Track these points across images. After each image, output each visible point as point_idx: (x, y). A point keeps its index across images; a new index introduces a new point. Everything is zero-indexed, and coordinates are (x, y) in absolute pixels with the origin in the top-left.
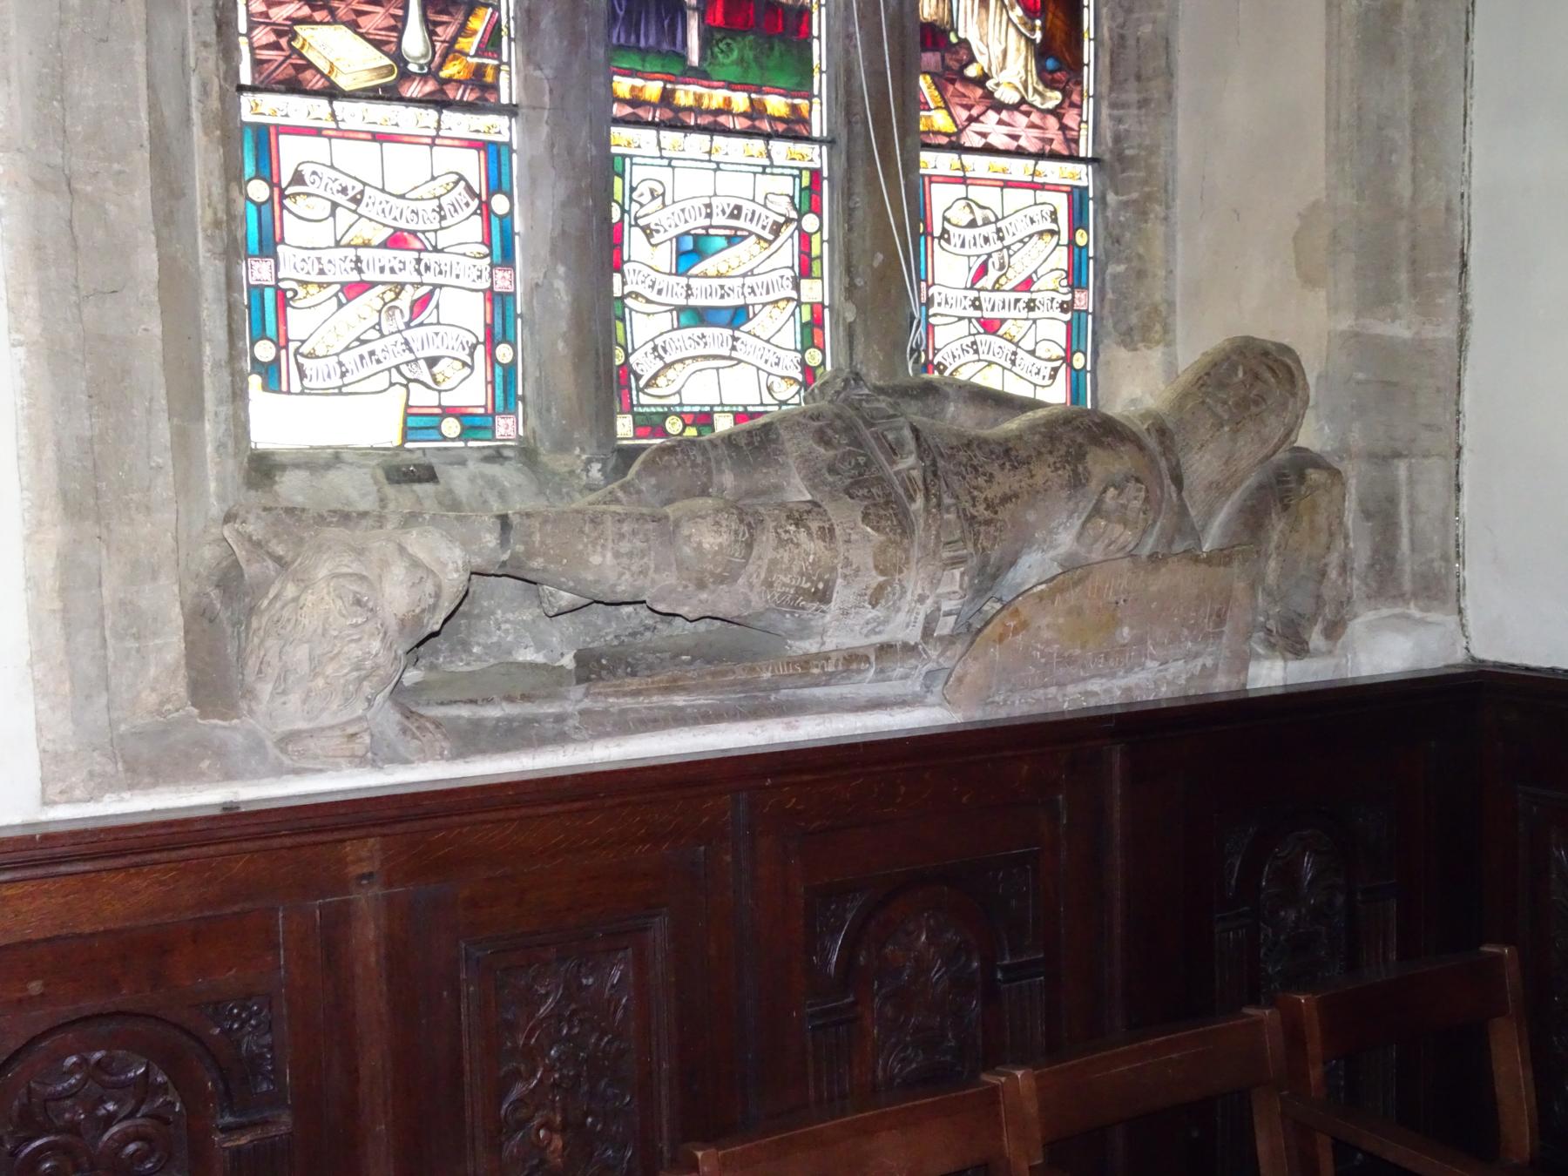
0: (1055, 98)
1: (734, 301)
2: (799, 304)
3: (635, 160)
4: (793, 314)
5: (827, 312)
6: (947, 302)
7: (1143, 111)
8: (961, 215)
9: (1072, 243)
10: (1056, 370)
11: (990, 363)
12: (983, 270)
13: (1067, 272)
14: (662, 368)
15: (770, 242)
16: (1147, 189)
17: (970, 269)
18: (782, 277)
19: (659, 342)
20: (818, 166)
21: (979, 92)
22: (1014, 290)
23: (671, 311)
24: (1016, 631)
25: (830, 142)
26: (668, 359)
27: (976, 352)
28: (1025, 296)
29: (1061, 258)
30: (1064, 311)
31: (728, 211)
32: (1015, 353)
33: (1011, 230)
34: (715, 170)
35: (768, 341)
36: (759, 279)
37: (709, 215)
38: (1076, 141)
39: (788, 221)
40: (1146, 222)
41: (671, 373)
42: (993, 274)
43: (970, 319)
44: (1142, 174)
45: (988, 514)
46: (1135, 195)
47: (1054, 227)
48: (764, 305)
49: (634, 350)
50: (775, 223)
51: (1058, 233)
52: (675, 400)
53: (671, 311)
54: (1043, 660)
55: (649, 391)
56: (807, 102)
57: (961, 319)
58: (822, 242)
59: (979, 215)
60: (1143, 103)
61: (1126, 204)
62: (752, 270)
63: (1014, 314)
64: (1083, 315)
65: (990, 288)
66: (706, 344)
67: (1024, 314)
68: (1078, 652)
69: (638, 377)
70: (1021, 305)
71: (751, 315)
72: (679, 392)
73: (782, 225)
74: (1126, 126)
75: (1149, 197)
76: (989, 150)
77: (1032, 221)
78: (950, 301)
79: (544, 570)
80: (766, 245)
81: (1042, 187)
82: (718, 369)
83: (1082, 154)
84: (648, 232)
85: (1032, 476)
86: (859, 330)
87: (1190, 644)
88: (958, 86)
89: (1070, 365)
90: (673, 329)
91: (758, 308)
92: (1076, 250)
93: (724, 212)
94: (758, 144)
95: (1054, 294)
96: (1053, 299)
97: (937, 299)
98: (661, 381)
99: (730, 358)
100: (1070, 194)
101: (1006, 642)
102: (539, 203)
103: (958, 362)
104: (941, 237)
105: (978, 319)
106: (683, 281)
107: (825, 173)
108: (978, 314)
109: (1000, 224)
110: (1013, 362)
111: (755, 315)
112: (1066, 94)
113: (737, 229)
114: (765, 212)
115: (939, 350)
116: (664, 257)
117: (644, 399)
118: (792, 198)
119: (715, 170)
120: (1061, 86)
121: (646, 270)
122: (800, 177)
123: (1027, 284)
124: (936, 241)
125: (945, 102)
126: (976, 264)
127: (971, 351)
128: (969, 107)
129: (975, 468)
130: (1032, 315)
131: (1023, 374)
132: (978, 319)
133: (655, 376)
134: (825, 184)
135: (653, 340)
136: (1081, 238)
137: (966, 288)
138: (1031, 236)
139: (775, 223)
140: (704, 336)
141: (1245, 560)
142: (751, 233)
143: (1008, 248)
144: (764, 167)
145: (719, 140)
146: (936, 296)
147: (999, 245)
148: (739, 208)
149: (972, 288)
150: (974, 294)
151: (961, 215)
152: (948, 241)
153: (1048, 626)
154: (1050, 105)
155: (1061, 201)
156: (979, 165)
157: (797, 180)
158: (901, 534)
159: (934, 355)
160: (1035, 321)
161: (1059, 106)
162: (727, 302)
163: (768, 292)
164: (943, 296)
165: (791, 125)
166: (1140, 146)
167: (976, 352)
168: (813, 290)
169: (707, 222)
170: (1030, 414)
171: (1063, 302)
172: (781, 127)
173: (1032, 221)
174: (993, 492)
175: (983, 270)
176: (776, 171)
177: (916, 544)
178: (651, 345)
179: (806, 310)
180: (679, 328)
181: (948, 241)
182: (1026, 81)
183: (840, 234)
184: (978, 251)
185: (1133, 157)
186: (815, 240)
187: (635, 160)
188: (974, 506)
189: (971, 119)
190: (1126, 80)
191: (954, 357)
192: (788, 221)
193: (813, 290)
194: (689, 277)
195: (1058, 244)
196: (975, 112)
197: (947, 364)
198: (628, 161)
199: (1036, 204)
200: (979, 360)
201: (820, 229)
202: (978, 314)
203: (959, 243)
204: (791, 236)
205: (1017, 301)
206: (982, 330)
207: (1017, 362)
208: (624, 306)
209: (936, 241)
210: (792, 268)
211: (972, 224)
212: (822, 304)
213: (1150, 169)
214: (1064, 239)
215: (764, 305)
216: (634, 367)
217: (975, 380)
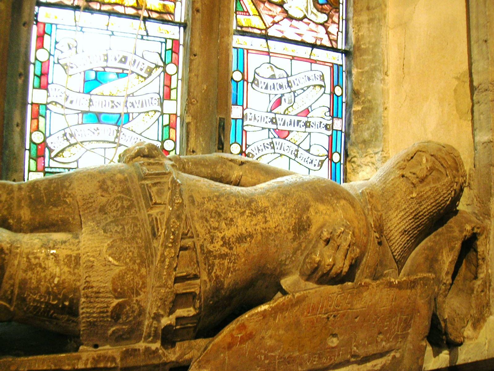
0: (323, 18)
1: (121, 109)
2: (162, 114)
3: (58, 26)
4: (158, 120)
5: (178, 119)
6: (255, 118)
7: (371, 25)
8: (265, 71)
9: (333, 94)
10: (322, 162)
11: (281, 155)
12: (279, 102)
13: (330, 109)
14: (69, 146)
15: (145, 78)
16: (373, 65)
17: (270, 101)
18: (152, 98)
19: (68, 131)
20: (178, 38)
21: (279, 9)
22: (297, 115)
23: (78, 114)
24: (243, 340)
25: (184, 25)
26: (73, 141)
27: (273, 148)
28: (304, 119)
29: (326, 100)
30: (327, 129)
31: (118, 59)
32: (297, 151)
33: (296, 82)
34: (110, 35)
35: (140, 134)
36: (137, 99)
37: (106, 61)
38: (336, 41)
39: (157, 66)
40: (373, 82)
41: (72, 149)
42: (284, 105)
43: (269, 130)
44: (370, 57)
45: (225, 250)
46: (367, 68)
47: (322, 84)
48: (140, 113)
49: (50, 135)
50: (149, 67)
51: (325, 87)
52: (74, 165)
53: (78, 114)
54: (267, 362)
55: (57, 159)
56: (173, 4)
57: (263, 128)
58: (178, 80)
59: (278, 73)
60: (371, 21)
61: (362, 73)
62: (133, 94)
63: (297, 128)
64: (339, 133)
65: (282, 113)
66: (99, 134)
67: (303, 129)
68: (297, 354)
69: (51, 151)
70: (301, 124)
71: (131, 119)
72: (77, 161)
73: (153, 69)
74: (362, 33)
75: (374, 69)
76: (284, 40)
77: (309, 79)
78: (257, 118)
79: (481, 215)
80: (143, 79)
81: (315, 62)
82: (105, 148)
83: (339, 47)
84: (65, 67)
85: (266, 222)
86: (192, 128)
87: (384, 343)
88: (267, 5)
89: (331, 160)
90: (78, 124)
91: (135, 115)
92: (335, 97)
93: (116, 59)
94: (138, 23)
95: (322, 120)
96: (321, 122)
97: (249, 117)
98: (65, 153)
99: (114, 143)
100: (332, 68)
101: (235, 348)
102: (223, 124)
103: (261, 153)
104: (252, 83)
105: (274, 130)
106: (88, 96)
107: (181, 42)
108: (274, 127)
109: (289, 79)
110: (296, 156)
111: (133, 119)
112: (329, 16)
113: (123, 70)
114: (142, 61)
115: (249, 146)
116: (77, 83)
117: (53, 164)
118: (160, 55)
119: (110, 35)
120: (327, 12)
121: (64, 90)
122: (166, 43)
123: (307, 112)
124: (249, 84)
125: (259, 12)
126: (274, 99)
127: (270, 147)
128: (273, 17)
129: (219, 215)
130: (308, 130)
131: (302, 162)
132: (274, 130)
133: (62, 151)
134: (181, 48)
135: (64, 129)
136: (338, 91)
137: (267, 112)
138: (308, 87)
139: (149, 67)
140: (98, 129)
141: (425, 285)
142: (133, 72)
143: (294, 92)
144: (142, 36)
145: (113, 18)
146: (249, 115)
147: (288, 90)
148: (126, 58)
149: (271, 112)
150: (272, 115)
151: (265, 71)
152: (257, 85)
153: (271, 337)
154: (322, 21)
155: (326, 71)
156: (275, 46)
157: (164, 44)
158: (139, 264)
159: (246, 148)
160: (310, 133)
161: (326, 22)
162: (115, 110)
163: (142, 106)
164: (253, 115)
165: (162, 15)
166: (369, 43)
167: (273, 148)
168: (171, 107)
169: (104, 64)
170: (279, 179)
171: (327, 125)
172: (155, 15)
173: (309, 79)
174: (229, 233)
175: (279, 102)
176: (149, 38)
177: (152, 273)
178: (63, 132)
179: (166, 118)
180: (82, 124)
181: (257, 85)
182: (307, 7)
183: (187, 76)
184: (276, 92)
185: (365, 49)
186: (174, 79)
187: (58, 26)
188: (212, 242)
189: (274, 23)
190: (361, 10)
191: (259, 150)
192: (157, 66)
193: (171, 107)
194: (91, 95)
195: (324, 93)
196: (276, 19)
197: (254, 154)
198: (54, 26)
199: (311, 70)
200: (275, 153)
201: (177, 72)
202: (274, 127)
203: (264, 87)
204: (159, 76)
205: (299, 122)
206: (277, 136)
207: (299, 156)
208: (47, 109)
209: (249, 84)
210: (159, 94)
211: (273, 77)
212: (176, 114)
213: (375, 55)
214: (328, 90)
215: (140, 113)
216: (50, 145)
217: (272, 165)
